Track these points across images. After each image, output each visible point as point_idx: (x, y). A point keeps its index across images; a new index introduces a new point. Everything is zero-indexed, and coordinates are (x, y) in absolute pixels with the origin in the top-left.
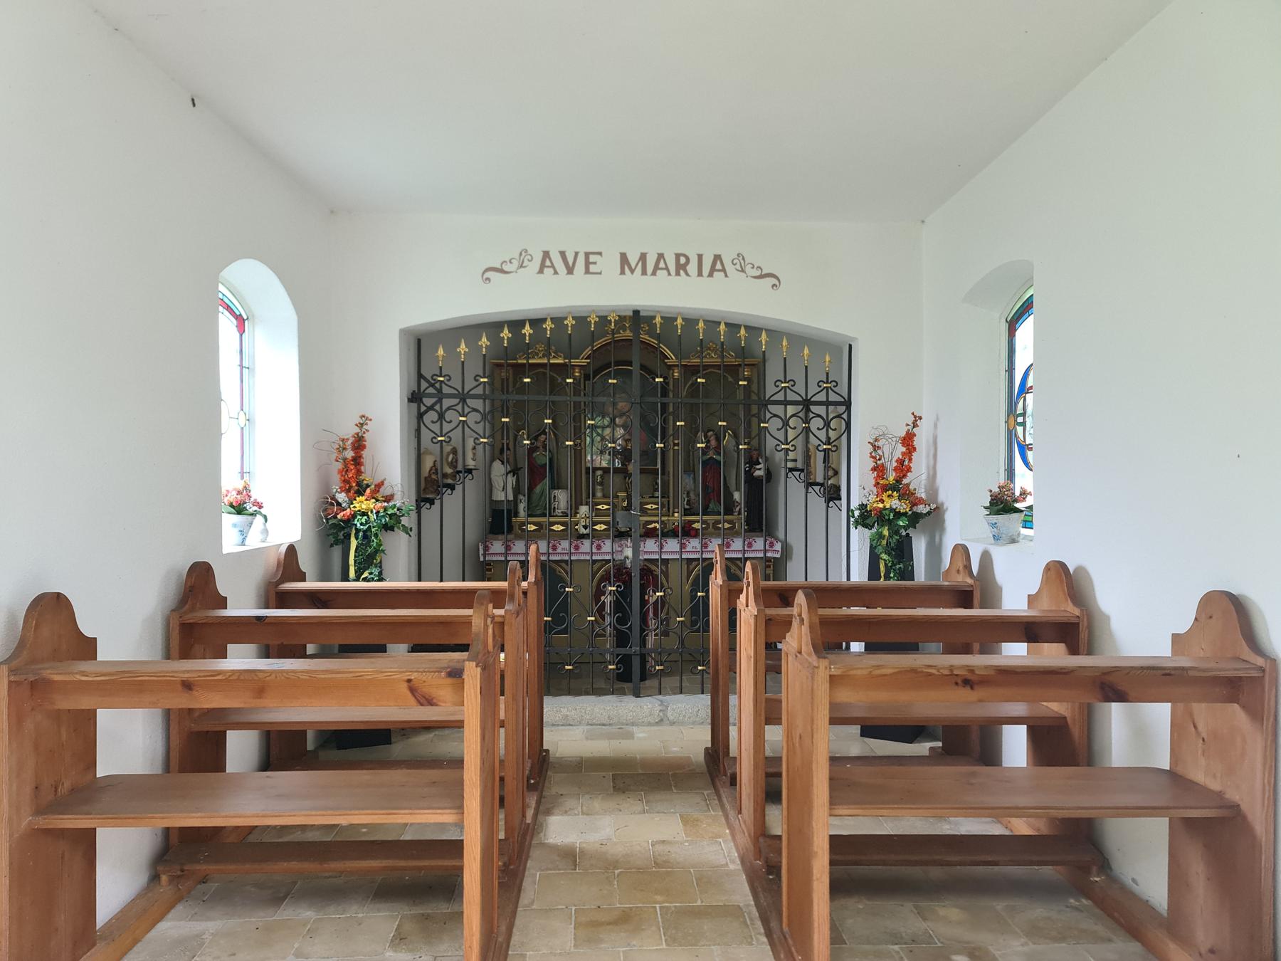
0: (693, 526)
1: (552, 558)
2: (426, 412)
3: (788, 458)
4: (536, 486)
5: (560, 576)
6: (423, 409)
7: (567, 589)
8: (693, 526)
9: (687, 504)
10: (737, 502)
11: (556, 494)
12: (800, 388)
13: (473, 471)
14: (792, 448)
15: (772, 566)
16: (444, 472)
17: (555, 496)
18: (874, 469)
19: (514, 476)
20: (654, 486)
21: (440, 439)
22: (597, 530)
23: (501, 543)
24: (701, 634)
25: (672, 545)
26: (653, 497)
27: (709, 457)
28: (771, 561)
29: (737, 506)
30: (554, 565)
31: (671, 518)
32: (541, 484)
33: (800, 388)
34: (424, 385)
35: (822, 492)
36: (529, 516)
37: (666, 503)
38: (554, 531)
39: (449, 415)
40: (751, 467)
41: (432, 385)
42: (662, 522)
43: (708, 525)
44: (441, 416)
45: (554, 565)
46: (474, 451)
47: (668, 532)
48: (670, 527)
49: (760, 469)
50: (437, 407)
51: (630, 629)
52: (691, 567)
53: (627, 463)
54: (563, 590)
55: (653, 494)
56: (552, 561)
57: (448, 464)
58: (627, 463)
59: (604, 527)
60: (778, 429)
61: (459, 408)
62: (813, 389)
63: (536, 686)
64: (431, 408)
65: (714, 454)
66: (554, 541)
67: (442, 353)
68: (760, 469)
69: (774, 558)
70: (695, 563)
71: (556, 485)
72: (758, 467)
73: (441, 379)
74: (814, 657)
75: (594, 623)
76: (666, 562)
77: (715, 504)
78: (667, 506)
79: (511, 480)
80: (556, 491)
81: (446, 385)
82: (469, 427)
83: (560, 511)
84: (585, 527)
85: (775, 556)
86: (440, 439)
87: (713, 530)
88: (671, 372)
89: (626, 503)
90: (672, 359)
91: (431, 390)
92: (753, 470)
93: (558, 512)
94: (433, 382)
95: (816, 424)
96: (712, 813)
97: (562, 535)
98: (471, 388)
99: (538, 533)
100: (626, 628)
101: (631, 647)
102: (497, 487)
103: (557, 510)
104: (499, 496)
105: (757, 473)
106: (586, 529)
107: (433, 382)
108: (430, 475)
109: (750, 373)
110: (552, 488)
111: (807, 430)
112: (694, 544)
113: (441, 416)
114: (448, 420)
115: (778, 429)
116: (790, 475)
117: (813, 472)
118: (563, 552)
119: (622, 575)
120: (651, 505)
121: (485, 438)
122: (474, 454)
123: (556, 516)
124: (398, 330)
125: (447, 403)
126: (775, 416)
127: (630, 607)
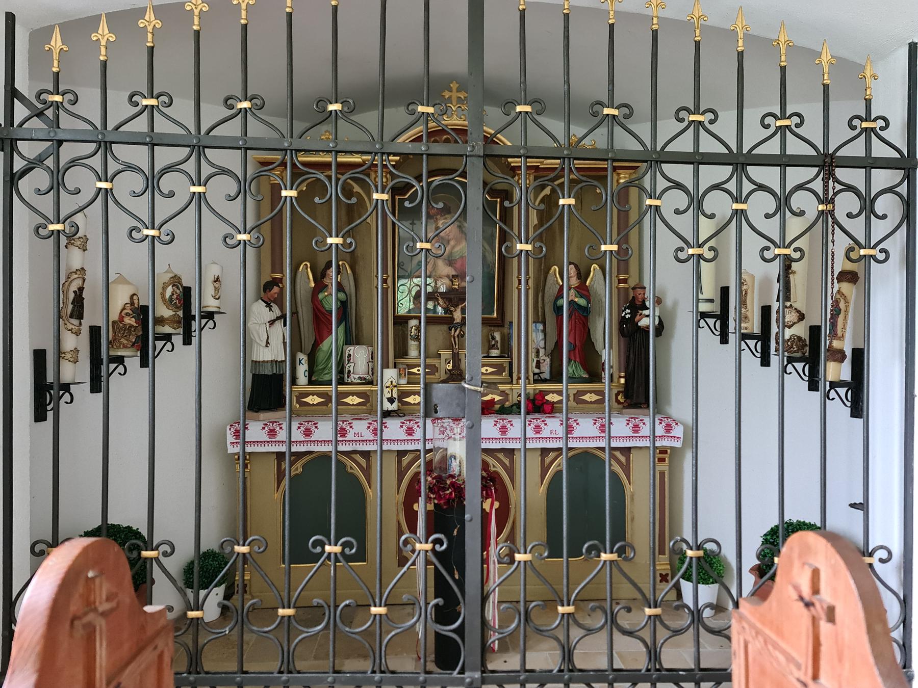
0: (547, 398)
1: (341, 448)
2: (24, 172)
3: (701, 296)
4: (322, 341)
5: (352, 474)
6: (19, 164)
7: (328, 548)
8: (547, 398)
9: (536, 367)
11: (351, 353)
12: (813, 130)
13: (215, 315)
14: (796, 255)
15: (667, 459)
16: (158, 314)
20: (489, 342)
21: (52, 227)
22: (409, 404)
23: (260, 425)
24: (564, 559)
25: (516, 426)
26: (488, 357)
28: (666, 452)
30: (345, 459)
31: (515, 387)
33: (813, 130)
34: (21, 111)
35: (759, 350)
36: (311, 382)
37: (507, 365)
38: (348, 404)
39: (73, 178)
40: (634, 314)
41: (40, 114)
42: (503, 393)
44: (57, 184)
45: (345, 459)
46: (217, 285)
47: (512, 406)
48: (513, 399)
49: (648, 316)
50: (50, 162)
51: (460, 631)
52: (548, 460)
53: (452, 309)
54: (319, 549)
55: (488, 352)
56: (343, 453)
57: (164, 301)
58: (452, 309)
60: (768, 216)
61: (96, 162)
62: (840, 133)
64: (38, 161)
65: (576, 297)
66: (343, 421)
67: (59, 43)
68: (648, 316)
69: (672, 448)
70: (552, 455)
71: (353, 338)
72: (646, 312)
73: (58, 98)
75: (384, 618)
76: (510, 452)
77: (576, 368)
78: (507, 369)
79: (280, 333)
80: (352, 348)
81: (67, 111)
82: (117, 202)
83: (357, 376)
84: (391, 400)
85: (673, 445)
86: (52, 227)
89: (451, 365)
91: (36, 123)
92: (638, 317)
93: (354, 378)
94: (40, 106)
95: (846, 203)
96: (457, 448)
97: (358, 413)
98: (122, 119)
99: (324, 408)
100: (453, 631)
101: (462, 672)
102: (258, 340)
103: (352, 375)
104: (264, 354)
105: (643, 322)
107: (40, 106)
108: (121, 319)
110: (346, 344)
111: (827, 216)
112: (553, 426)
113: (57, 184)
114: (71, 187)
115: (768, 216)
116: (702, 323)
118: (357, 438)
119: (444, 489)
120: (485, 368)
121: (153, 228)
122: (217, 289)
123: (352, 384)
125: (68, 152)
126: (761, 187)
127: (461, 584)
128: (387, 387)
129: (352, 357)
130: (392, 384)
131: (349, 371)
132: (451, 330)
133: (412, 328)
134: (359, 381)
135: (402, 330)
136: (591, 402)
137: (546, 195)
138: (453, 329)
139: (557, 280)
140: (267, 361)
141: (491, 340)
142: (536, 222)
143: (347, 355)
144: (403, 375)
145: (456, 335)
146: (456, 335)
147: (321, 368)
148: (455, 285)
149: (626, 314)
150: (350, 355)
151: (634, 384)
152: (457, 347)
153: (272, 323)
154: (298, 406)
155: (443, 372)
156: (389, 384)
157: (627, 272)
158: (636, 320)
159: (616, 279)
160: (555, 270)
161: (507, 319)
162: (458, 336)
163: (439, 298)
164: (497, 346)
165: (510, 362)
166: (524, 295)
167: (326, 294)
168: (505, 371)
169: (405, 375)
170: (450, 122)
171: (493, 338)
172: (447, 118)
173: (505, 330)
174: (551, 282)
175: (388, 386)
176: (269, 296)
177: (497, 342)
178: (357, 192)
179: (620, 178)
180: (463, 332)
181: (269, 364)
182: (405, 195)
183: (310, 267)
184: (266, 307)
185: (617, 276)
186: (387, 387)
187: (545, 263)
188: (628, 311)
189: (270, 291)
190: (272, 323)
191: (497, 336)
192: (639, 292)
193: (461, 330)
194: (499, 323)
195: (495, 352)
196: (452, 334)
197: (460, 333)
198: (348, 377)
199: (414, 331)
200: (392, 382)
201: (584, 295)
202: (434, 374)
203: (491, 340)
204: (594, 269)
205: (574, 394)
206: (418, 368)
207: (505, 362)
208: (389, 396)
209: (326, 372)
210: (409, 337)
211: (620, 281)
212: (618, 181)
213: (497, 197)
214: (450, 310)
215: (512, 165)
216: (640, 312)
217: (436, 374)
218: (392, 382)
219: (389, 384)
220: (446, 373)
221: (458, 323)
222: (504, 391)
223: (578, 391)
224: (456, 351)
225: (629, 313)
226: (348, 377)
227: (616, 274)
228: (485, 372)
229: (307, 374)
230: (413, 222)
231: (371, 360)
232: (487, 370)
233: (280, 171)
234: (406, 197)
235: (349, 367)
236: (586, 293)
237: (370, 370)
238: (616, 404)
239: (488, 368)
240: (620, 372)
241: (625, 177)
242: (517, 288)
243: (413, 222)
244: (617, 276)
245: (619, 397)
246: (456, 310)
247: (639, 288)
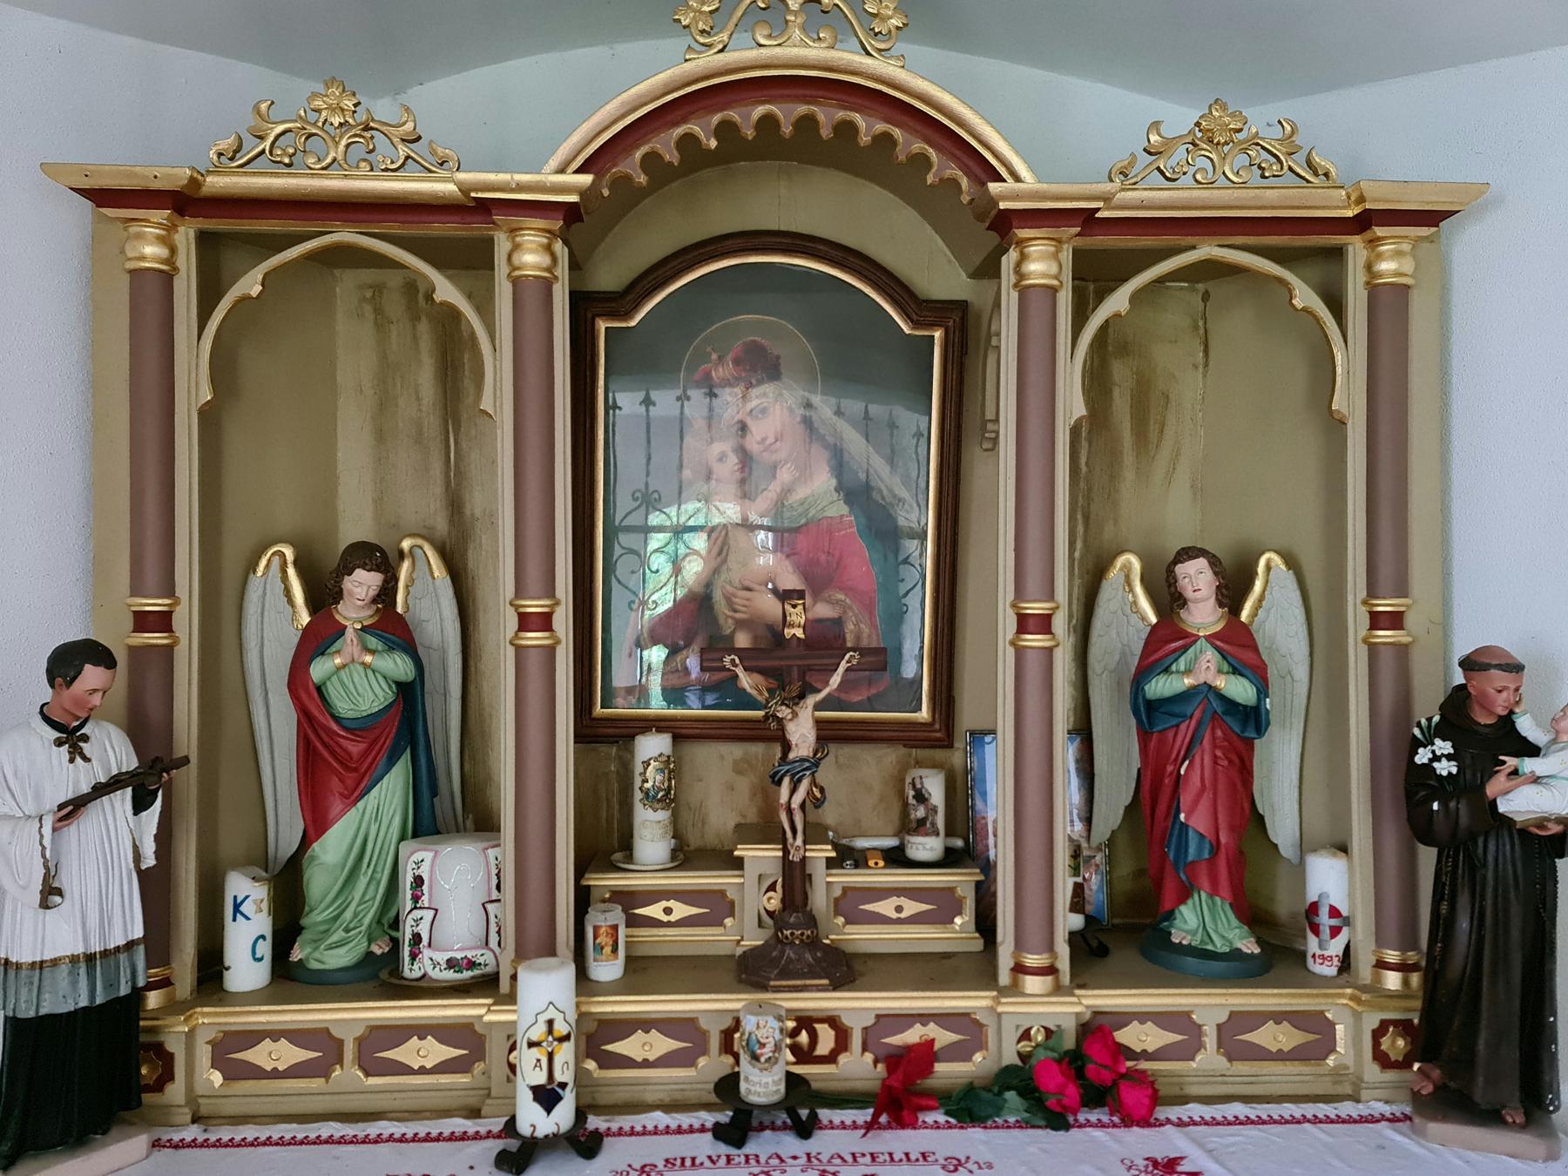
10: (1334, 913)
11: (424, 872)
17: (419, 881)
18: (716, 396)
19: (140, 805)
27: (1188, 681)
29: (1335, 932)
31: (1008, 1006)
32: (352, 815)
43: (1195, 1031)
53: (784, 712)
59: (661, 1045)
63: (896, 198)
74: (814, 419)
78: (969, 905)
83: (441, 958)
84: (547, 1097)
87: (1221, 1062)
88: (1013, 255)
90: (1017, 179)
99: (316, 1084)
103: (426, 953)
106: (549, 1110)
109: (1408, 265)
117: (785, 411)
120: (894, 901)
124: (1526, 664)
128: (531, 1044)
129: (425, 887)
130: (550, 1031)
131: (417, 938)
132: (779, 783)
133: (647, 764)
134: (450, 975)
135: (620, 758)
136: (1280, 1056)
137: (1117, 315)
138: (786, 781)
139: (1135, 603)
140: (55, 962)
141: (912, 801)
142: (1079, 409)
143: (409, 879)
144: (608, 950)
145: (795, 804)
146: (795, 804)
147: (320, 918)
148: (792, 626)
149: (1436, 758)
150: (419, 881)
151: (1475, 1033)
152: (799, 841)
153: (73, 808)
154: (217, 1078)
155: (750, 920)
156: (538, 1032)
157: (1402, 590)
158: (1491, 789)
159: (1363, 610)
160: (1127, 569)
161: (968, 717)
162: (803, 806)
163: (740, 671)
164: (933, 824)
165: (978, 884)
166: (934, 542)
167: (338, 661)
168: (960, 913)
169: (615, 950)
170: (778, 50)
171: (921, 797)
172: (770, 36)
173: (956, 758)
174: (1113, 606)
175: (535, 1038)
176: (68, 705)
177: (934, 810)
178: (445, 304)
179: (1380, 256)
180: (822, 790)
181: (64, 969)
182: (627, 315)
183: (295, 563)
184: (59, 743)
185: (1365, 603)
186: (531, 1044)
187: (1085, 541)
188: (1443, 747)
189: (69, 684)
190: (73, 808)
191: (935, 788)
192: (1499, 685)
193: (814, 783)
194: (938, 740)
195: (926, 847)
196: (784, 798)
197: (809, 793)
198: (414, 956)
199: (654, 777)
200: (550, 1023)
201: (1246, 665)
202: (721, 924)
203: (912, 801)
204: (1268, 568)
205: (1219, 1027)
206: (664, 904)
207: (961, 880)
208: (540, 1078)
209: (335, 938)
210: (638, 795)
211: (1377, 620)
212: (1369, 267)
213: (932, 325)
214: (774, 716)
215: (1002, 206)
216: (1511, 762)
217: (728, 921)
218: (550, 1023)
219: (538, 1032)
220: (760, 924)
221: (803, 760)
222: (967, 1015)
223: (1232, 1014)
224: (795, 857)
225: (1449, 757)
226: (414, 956)
227: (1363, 594)
228: (894, 915)
229: (265, 949)
230: (711, 391)
231: (495, 895)
232: (899, 909)
233: (159, 225)
234: (633, 323)
235: (418, 921)
236: (1248, 656)
237: (493, 929)
238: (1376, 1068)
239: (903, 901)
240: (1380, 942)
241: (1398, 254)
242: (1012, 643)
243: (711, 391)
244: (1365, 603)
245: (1385, 1043)
246: (795, 715)
247: (1499, 667)
